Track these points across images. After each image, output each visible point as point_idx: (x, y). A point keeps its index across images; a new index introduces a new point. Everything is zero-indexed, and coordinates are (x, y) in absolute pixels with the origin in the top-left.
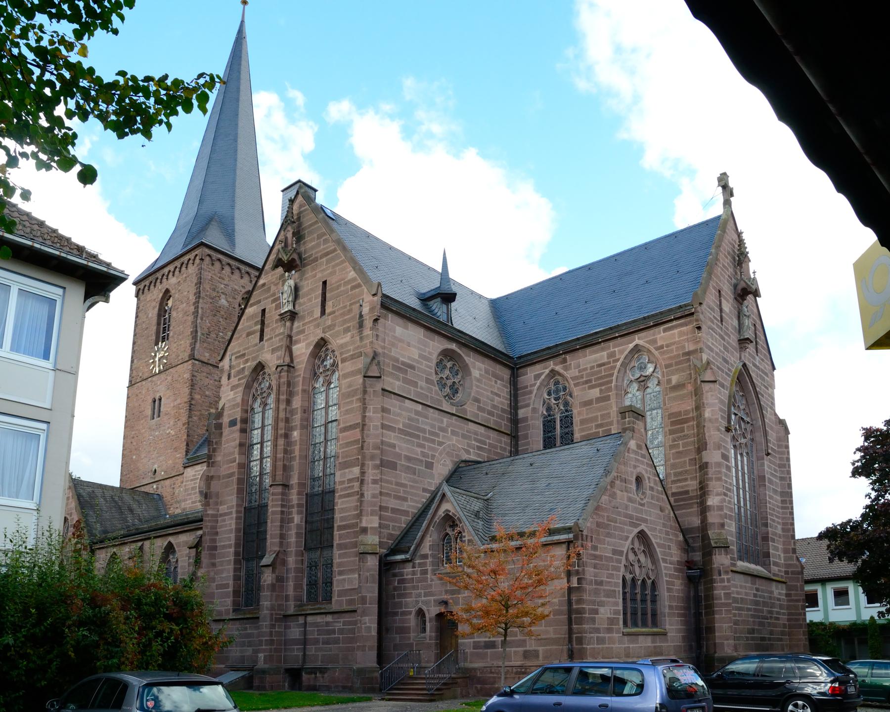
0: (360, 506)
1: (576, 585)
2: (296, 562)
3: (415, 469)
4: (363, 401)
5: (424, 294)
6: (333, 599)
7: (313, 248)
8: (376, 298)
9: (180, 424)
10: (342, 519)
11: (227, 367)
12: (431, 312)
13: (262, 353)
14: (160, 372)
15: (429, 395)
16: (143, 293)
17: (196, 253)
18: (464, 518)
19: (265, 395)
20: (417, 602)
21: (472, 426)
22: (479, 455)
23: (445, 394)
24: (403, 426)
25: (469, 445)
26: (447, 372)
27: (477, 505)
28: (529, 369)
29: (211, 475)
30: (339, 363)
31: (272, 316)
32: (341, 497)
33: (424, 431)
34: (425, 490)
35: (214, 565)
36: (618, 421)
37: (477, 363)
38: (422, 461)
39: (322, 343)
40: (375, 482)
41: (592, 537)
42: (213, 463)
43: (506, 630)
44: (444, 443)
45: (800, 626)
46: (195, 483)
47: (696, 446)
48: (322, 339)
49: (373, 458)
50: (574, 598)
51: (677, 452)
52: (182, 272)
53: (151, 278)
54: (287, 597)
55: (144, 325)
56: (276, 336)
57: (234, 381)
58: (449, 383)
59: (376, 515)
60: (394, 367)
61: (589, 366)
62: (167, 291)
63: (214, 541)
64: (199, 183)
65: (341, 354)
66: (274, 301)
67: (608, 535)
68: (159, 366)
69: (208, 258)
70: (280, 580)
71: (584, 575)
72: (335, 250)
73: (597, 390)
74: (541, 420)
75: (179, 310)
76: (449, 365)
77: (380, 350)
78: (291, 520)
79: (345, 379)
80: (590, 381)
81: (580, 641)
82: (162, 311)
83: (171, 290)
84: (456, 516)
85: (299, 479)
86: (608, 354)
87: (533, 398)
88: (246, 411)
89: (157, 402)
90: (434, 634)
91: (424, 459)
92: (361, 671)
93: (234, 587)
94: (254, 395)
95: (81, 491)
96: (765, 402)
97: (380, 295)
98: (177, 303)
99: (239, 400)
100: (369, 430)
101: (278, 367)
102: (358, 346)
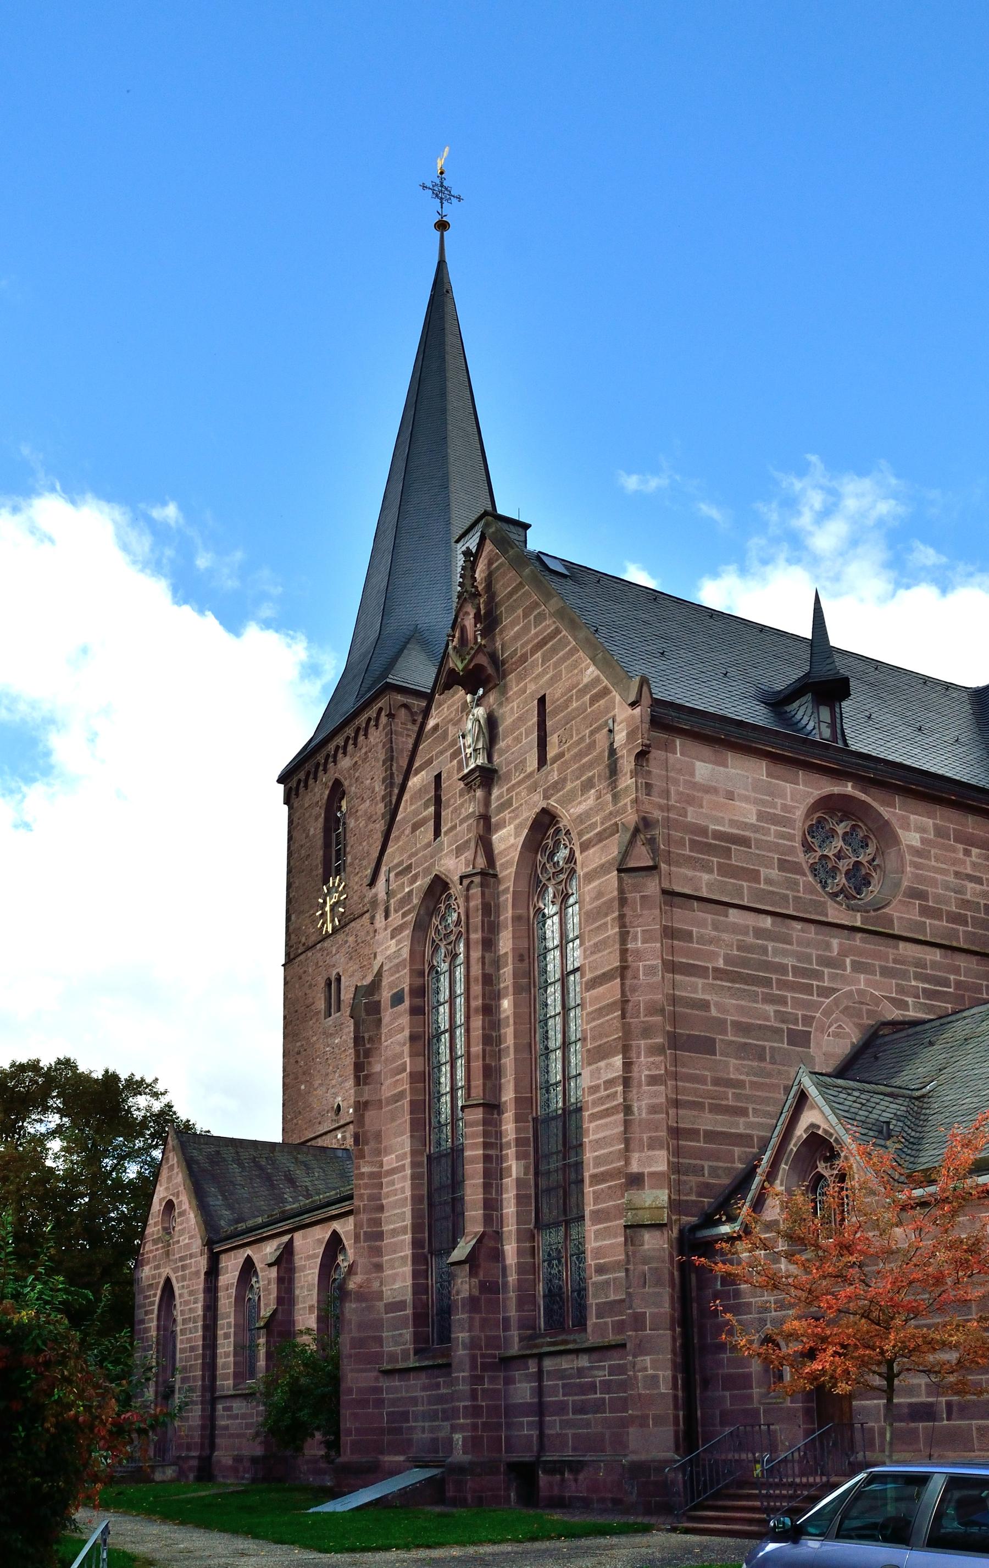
2: (520, 1252)
3: (764, 1048)
6: (589, 1323)
7: (517, 637)
8: (638, 710)
10: (598, 1161)
11: (382, 895)
13: (440, 859)
14: (335, 930)
17: (379, 705)
19: (453, 938)
20: (763, 1322)
22: (930, 1009)
23: (836, 889)
24: (726, 963)
25: (901, 990)
26: (839, 843)
29: (364, 1099)
30: (577, 854)
31: (452, 786)
32: (594, 1117)
33: (782, 969)
37: (912, 817)
38: (778, 1031)
39: (546, 820)
40: (653, 1080)
42: (367, 1077)
43: (890, 1377)
44: (835, 990)
48: (544, 811)
49: (647, 1032)
52: (359, 745)
53: (307, 766)
54: (506, 1320)
56: (461, 822)
58: (844, 865)
59: (661, 1148)
60: (694, 845)
63: (378, 1222)
64: (381, 580)
65: (580, 834)
68: (332, 921)
72: (557, 631)
75: (359, 813)
76: (841, 829)
77: (657, 814)
79: (590, 882)
83: (343, 780)
84: (831, 1135)
85: (516, 1091)
88: (421, 974)
91: (784, 1026)
92: (639, 1470)
93: (414, 1308)
94: (434, 941)
95: (195, 1153)
97: (646, 700)
99: (405, 953)
100: (636, 977)
101: (462, 878)
102: (611, 813)
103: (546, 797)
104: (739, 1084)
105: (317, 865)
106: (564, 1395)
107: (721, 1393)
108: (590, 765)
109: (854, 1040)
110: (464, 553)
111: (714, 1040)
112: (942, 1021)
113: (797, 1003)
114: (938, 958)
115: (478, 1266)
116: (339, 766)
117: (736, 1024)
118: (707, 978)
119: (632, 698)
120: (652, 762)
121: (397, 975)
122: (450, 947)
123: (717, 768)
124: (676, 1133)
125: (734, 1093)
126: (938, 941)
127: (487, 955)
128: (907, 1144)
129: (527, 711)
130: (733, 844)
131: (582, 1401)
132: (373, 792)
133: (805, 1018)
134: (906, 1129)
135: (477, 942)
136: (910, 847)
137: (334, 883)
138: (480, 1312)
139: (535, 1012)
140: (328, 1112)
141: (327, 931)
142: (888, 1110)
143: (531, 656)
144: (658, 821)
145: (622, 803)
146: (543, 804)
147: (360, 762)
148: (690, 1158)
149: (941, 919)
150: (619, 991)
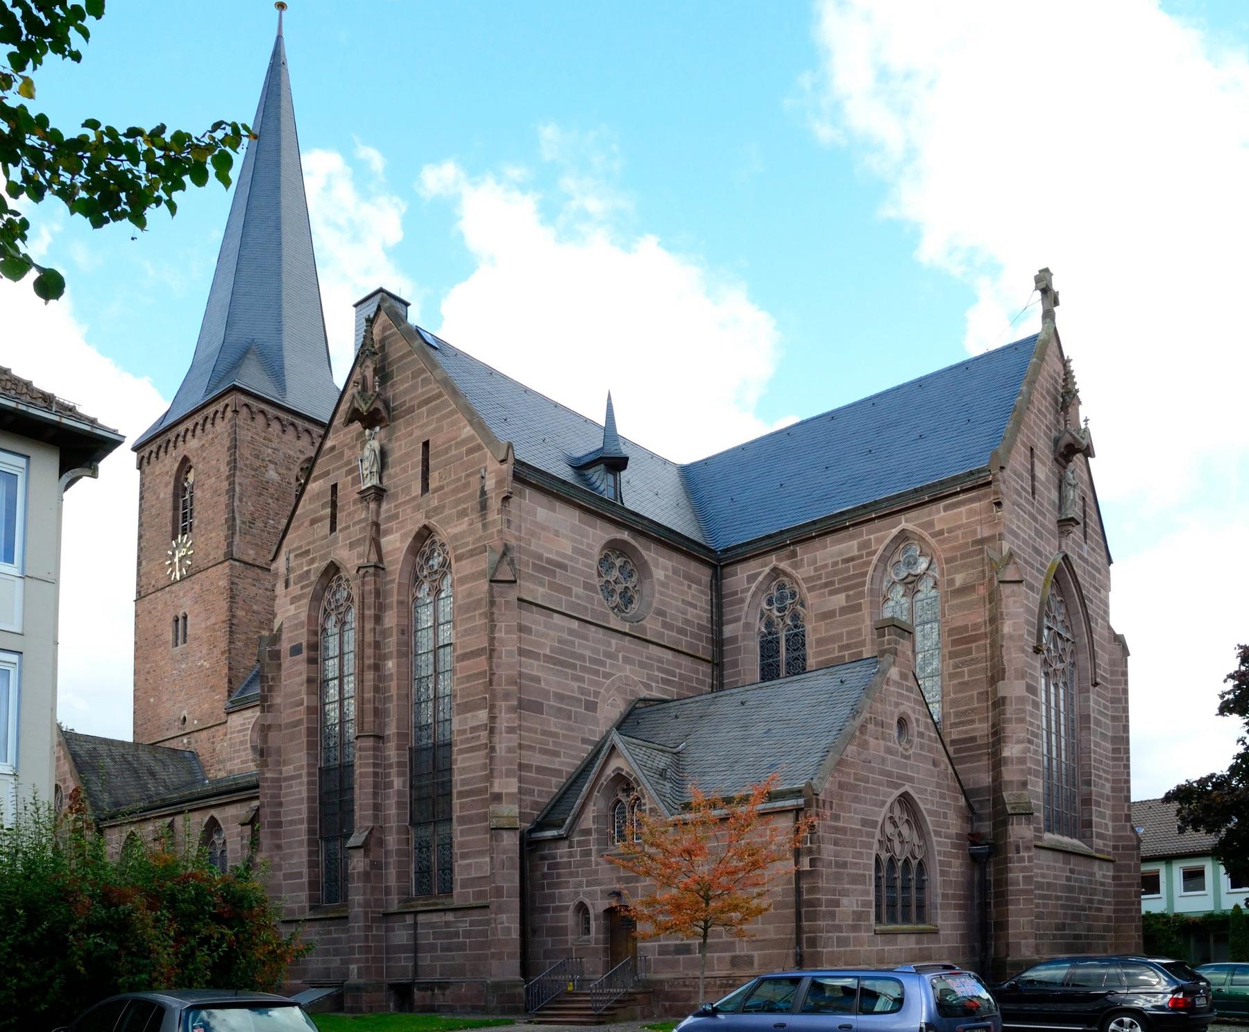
0: (490, 765)
2: (399, 842)
4: (491, 616)
5: (579, 459)
7: (406, 392)
8: (505, 466)
9: (217, 652)
10: (464, 782)
11: (282, 570)
12: (590, 485)
13: (335, 550)
14: (182, 578)
18: (643, 779)
19: (342, 609)
20: (577, 894)
22: (665, 691)
23: (614, 605)
24: (551, 651)
25: (649, 677)
26: (615, 573)
27: (662, 761)
28: (739, 567)
29: (267, 723)
30: (453, 562)
31: (348, 494)
32: (461, 752)
33: (582, 658)
34: (584, 741)
35: (279, 847)
36: (872, 640)
38: (580, 700)
39: (426, 533)
40: (511, 730)
41: (831, 802)
42: (269, 706)
43: (705, 929)
45: (1132, 919)
46: (244, 736)
47: (989, 674)
48: (425, 527)
49: (507, 696)
50: (805, 885)
51: (959, 683)
52: (206, 432)
55: (154, 511)
56: (355, 524)
57: (295, 589)
58: (619, 588)
59: (514, 776)
61: (830, 561)
62: (185, 459)
63: (278, 814)
65: (455, 549)
66: (349, 472)
67: (856, 799)
68: (180, 570)
69: (245, 410)
70: (376, 866)
71: (819, 853)
72: (440, 395)
73: (843, 596)
75: (205, 487)
77: (513, 542)
78: (389, 785)
80: (832, 583)
81: (813, 942)
84: (631, 776)
85: (398, 728)
86: (859, 544)
87: (746, 608)
88: (316, 633)
89: (181, 622)
91: (583, 697)
92: (497, 986)
94: (325, 610)
95: (77, 748)
96: (1094, 611)
97: (511, 461)
99: (304, 617)
102: (481, 537)
103: (427, 517)
104: (555, 735)
105: (166, 524)
106: (884, 950)
107: (545, 938)
108: (465, 500)
111: (542, 704)
112: (682, 702)
113: (592, 682)
114: (670, 658)
115: (370, 850)
116: (188, 445)
117: (556, 694)
118: (539, 660)
119: (502, 457)
120: (512, 505)
121: (296, 633)
122: (340, 616)
123: (550, 513)
127: (377, 627)
129: (414, 450)
131: (448, 943)
132: (218, 471)
135: (370, 617)
136: (658, 579)
137: (182, 540)
138: (370, 882)
139: (411, 672)
140: (175, 721)
141: (175, 578)
143: (418, 409)
147: (207, 445)
148: (528, 783)
149: (673, 631)
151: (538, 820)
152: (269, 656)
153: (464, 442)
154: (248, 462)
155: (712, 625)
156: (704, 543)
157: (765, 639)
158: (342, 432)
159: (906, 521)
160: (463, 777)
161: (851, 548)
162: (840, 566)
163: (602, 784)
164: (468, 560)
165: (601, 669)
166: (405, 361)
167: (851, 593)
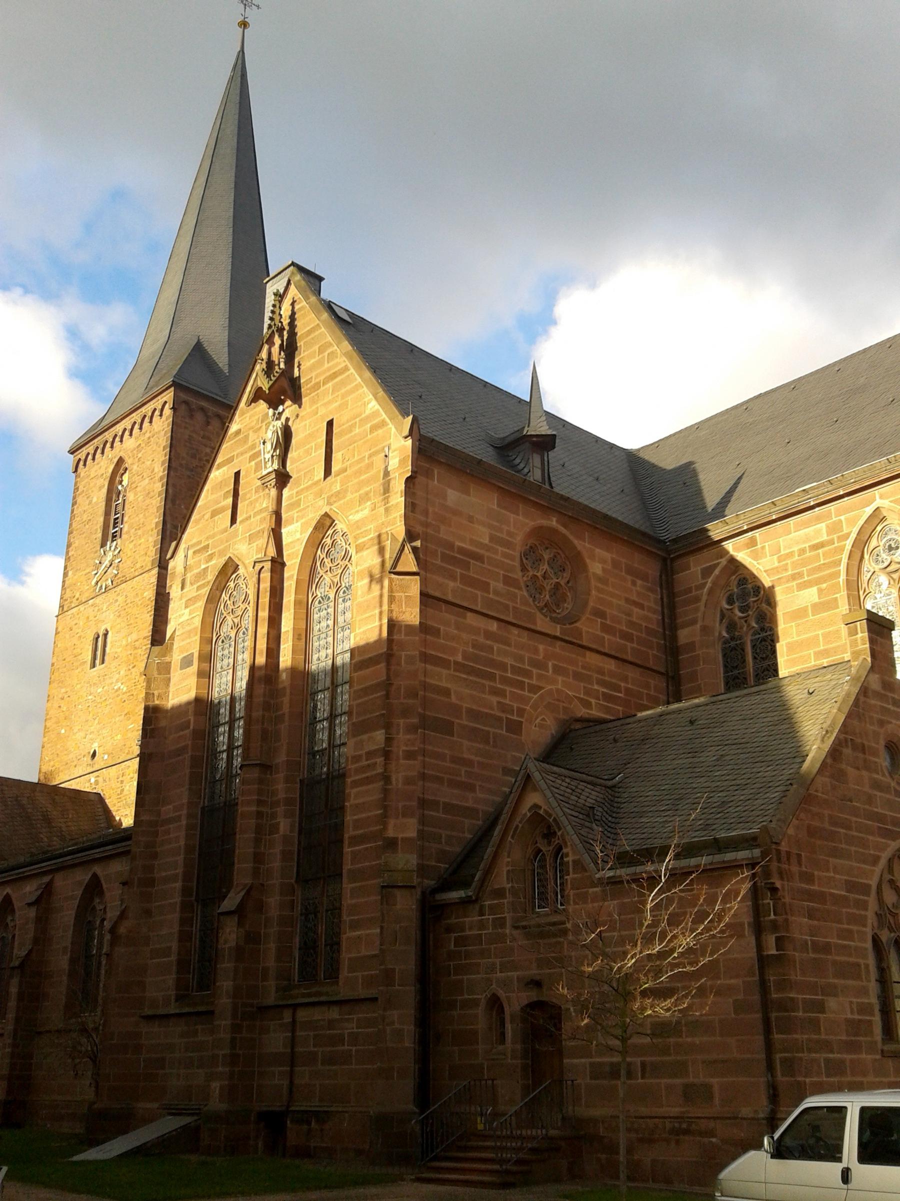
1: (774, 952)
5: (504, 438)
7: (312, 368)
12: (513, 467)
13: (235, 543)
15: (511, 604)
16: (85, 465)
17: (165, 399)
18: (563, 819)
21: (593, 659)
22: (608, 710)
23: (542, 604)
25: (588, 692)
27: (590, 796)
28: (691, 559)
31: (249, 483)
32: (356, 784)
33: (503, 666)
34: (507, 771)
37: (597, 550)
38: (500, 719)
39: (328, 522)
40: (409, 755)
41: (799, 856)
44: (541, 688)
48: (326, 515)
49: (406, 712)
50: (772, 978)
52: (144, 430)
55: (85, 517)
58: (548, 585)
60: (445, 558)
61: (796, 549)
62: (121, 461)
65: (356, 538)
66: (252, 458)
67: (835, 853)
69: (183, 407)
70: (253, 938)
71: (787, 931)
73: (814, 590)
74: (719, 647)
75: (138, 489)
78: (274, 828)
80: (800, 575)
81: (790, 1066)
82: (113, 493)
83: (126, 458)
84: (550, 816)
86: (827, 526)
87: (702, 608)
89: (100, 640)
90: (519, 1047)
91: (503, 715)
93: (179, 954)
98: (136, 478)
99: (197, 622)
100: (399, 664)
103: (329, 504)
106: (314, 1046)
108: (368, 482)
109: (553, 732)
110: (275, 294)
117: (470, 711)
118: (449, 669)
121: (188, 641)
124: (423, 803)
125: (466, 771)
126: (613, 653)
128: (606, 827)
130: (473, 559)
133: (519, 709)
134: (605, 814)
136: (594, 574)
140: (84, 756)
142: (591, 796)
144: (419, 534)
145: (392, 517)
146: (326, 509)
147: (143, 445)
150: (385, 674)
151: (445, 876)
152: (158, 669)
153: (368, 418)
154: (184, 462)
155: (664, 629)
156: (651, 533)
157: (727, 645)
158: (248, 415)
159: (881, 497)
160: (355, 817)
161: (818, 532)
162: (808, 554)
163: (517, 826)
164: (369, 551)
165: (526, 680)
166: (312, 336)
167: (824, 585)
